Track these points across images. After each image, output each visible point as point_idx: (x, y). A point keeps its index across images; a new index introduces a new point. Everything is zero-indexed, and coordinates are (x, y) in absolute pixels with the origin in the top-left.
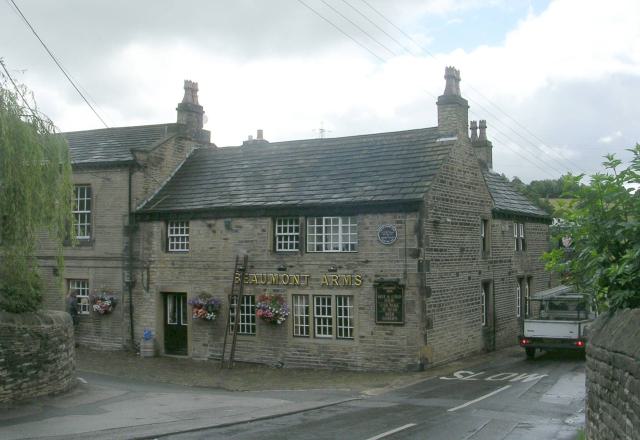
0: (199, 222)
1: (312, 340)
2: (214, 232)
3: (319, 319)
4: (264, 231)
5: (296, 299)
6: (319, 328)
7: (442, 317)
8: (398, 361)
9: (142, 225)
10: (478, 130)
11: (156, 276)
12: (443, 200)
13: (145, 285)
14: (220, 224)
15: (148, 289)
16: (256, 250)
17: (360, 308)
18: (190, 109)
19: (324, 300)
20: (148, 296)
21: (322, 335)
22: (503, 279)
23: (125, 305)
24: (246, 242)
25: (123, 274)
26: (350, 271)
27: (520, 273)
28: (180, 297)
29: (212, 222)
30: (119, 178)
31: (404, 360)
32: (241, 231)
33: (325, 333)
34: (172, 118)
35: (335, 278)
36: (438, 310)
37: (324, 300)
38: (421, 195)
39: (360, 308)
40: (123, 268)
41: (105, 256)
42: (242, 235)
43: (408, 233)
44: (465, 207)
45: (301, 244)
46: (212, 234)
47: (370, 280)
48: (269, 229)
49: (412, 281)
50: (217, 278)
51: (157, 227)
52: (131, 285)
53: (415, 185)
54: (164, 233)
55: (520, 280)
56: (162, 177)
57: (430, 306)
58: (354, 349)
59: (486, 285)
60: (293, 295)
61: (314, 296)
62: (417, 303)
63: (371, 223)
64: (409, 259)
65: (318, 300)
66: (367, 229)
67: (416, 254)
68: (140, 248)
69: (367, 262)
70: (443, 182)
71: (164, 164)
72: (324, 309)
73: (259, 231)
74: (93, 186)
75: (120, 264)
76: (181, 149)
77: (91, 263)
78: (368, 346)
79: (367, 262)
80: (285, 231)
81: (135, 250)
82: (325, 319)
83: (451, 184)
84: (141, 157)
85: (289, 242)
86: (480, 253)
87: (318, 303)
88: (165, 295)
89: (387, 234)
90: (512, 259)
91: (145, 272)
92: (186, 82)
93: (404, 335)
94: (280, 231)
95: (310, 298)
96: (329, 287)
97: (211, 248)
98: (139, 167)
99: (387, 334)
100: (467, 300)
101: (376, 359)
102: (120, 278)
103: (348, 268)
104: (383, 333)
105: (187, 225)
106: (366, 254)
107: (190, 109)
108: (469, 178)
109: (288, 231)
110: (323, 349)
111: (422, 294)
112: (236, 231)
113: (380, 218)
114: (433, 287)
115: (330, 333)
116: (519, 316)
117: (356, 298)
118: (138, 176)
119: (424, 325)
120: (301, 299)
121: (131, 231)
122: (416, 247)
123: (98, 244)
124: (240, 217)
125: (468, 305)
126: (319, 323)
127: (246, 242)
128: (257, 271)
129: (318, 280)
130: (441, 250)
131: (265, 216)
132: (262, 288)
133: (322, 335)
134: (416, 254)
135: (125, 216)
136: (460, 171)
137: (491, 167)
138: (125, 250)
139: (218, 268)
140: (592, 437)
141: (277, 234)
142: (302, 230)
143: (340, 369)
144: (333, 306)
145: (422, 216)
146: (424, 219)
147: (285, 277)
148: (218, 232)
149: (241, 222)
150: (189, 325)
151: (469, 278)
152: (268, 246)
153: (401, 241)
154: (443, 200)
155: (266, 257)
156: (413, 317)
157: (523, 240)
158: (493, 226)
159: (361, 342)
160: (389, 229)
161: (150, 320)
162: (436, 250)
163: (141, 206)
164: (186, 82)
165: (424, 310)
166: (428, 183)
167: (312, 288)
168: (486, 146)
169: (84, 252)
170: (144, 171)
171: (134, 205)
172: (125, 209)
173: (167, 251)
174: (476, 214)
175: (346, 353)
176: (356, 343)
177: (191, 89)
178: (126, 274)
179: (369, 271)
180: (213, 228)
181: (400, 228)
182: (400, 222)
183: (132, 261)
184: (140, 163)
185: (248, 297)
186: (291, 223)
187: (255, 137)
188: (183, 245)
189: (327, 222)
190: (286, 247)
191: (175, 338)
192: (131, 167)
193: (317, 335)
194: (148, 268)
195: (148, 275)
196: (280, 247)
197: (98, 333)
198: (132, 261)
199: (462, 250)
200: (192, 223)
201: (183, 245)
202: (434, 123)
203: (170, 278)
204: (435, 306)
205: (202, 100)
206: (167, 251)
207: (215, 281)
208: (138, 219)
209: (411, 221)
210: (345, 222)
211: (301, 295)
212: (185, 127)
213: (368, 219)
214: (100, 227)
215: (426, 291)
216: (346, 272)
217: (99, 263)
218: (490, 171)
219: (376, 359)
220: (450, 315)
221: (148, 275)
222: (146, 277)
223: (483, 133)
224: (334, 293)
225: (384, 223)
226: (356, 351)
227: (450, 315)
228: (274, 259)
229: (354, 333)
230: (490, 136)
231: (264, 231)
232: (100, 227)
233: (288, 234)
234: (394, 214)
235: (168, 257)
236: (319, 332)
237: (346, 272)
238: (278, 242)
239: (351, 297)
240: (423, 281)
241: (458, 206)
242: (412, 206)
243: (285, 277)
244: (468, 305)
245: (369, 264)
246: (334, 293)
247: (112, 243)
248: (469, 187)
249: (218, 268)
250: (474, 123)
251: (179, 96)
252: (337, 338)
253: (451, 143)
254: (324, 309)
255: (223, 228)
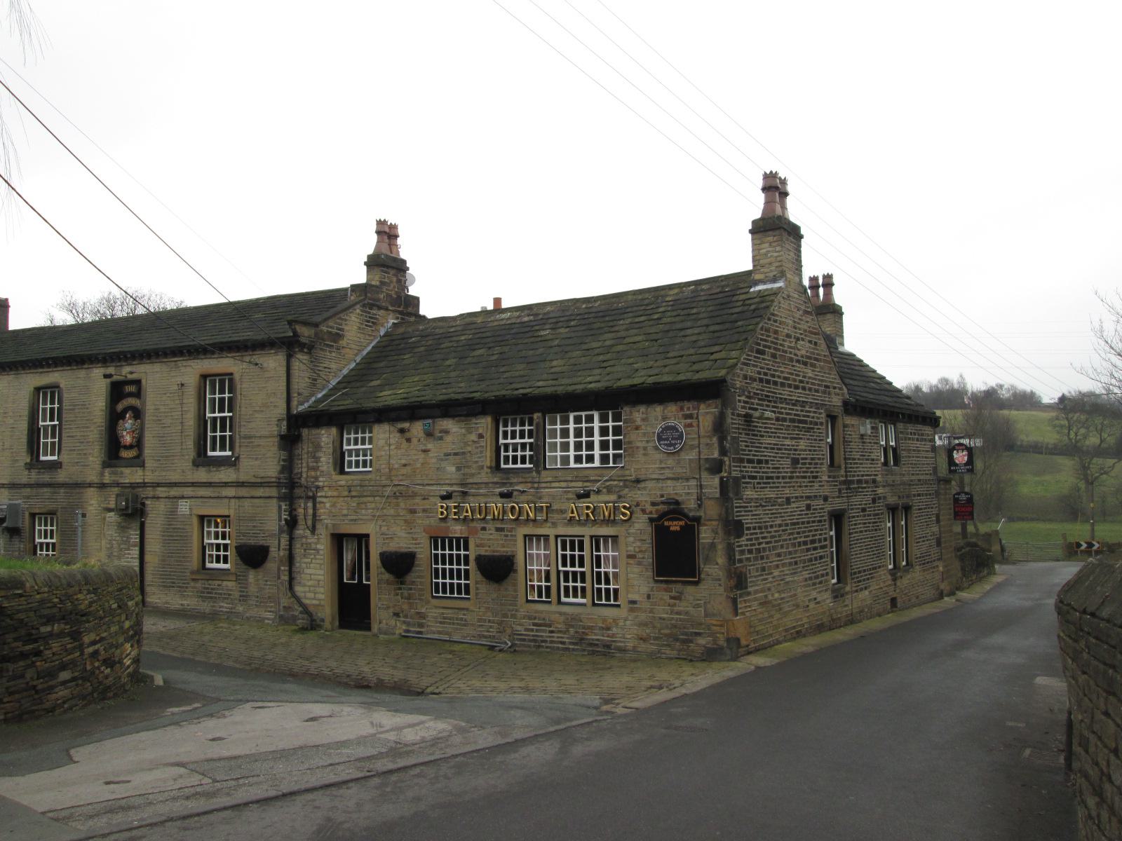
0: (386, 427)
1: (554, 607)
2: (409, 440)
3: (566, 573)
4: (481, 436)
5: (531, 540)
6: (567, 588)
7: (763, 569)
8: (691, 641)
9: (305, 432)
10: (821, 290)
11: (325, 507)
12: (761, 380)
13: (310, 523)
14: (417, 428)
15: (313, 530)
16: (469, 467)
17: (629, 557)
18: (387, 263)
19: (572, 543)
20: (312, 540)
21: (571, 600)
22: (864, 510)
23: (282, 553)
24: (456, 454)
25: (280, 507)
26: (613, 497)
27: (892, 500)
28: (362, 539)
29: (406, 425)
30: (274, 362)
31: (702, 641)
32: (449, 438)
33: (575, 596)
34: (359, 276)
35: (588, 508)
36: (756, 559)
37: (572, 543)
38: (723, 373)
39: (629, 557)
40: (280, 498)
41: (253, 480)
42: (450, 443)
43: (702, 433)
44: (797, 395)
45: (538, 459)
46: (405, 444)
47: (644, 511)
48: (489, 435)
49: (712, 510)
50: (413, 512)
51: (326, 436)
52: (292, 523)
53: (713, 357)
54: (337, 444)
55: (893, 510)
56: (339, 365)
57: (742, 552)
58: (621, 623)
59: (838, 518)
60: (525, 536)
61: (557, 537)
62: (720, 547)
63: (643, 420)
64: (705, 475)
65: (564, 543)
66: (637, 428)
67: (716, 467)
68: (302, 468)
69: (638, 481)
70: (763, 353)
71: (343, 343)
72: (573, 557)
73: (473, 437)
74: (237, 377)
75: (273, 492)
76: (373, 322)
77: (230, 492)
78: (643, 617)
79: (638, 481)
80: (513, 437)
81: (296, 471)
82: (574, 573)
83: (774, 356)
84: (305, 332)
85: (519, 453)
86: (825, 468)
87: (564, 549)
88: (339, 540)
89: (669, 436)
90: (879, 478)
91: (310, 505)
92: (381, 223)
93: (707, 595)
94: (505, 437)
95: (552, 540)
96: (580, 523)
97: (405, 465)
98: (302, 346)
99: (672, 598)
100: (805, 543)
101: (656, 638)
102: (273, 514)
103: (610, 490)
104: (666, 596)
105: (371, 432)
106: (636, 470)
107: (387, 263)
108: (804, 348)
109: (515, 437)
110: (572, 621)
111: (728, 533)
112: (441, 438)
113: (658, 410)
114: (747, 520)
115: (584, 596)
116: (891, 567)
117: (621, 539)
118: (301, 362)
119: (733, 583)
120: (606, 542)
121: (290, 440)
122: (716, 455)
123: (245, 463)
124: (446, 415)
125: (808, 550)
126: (566, 580)
127: (456, 454)
128: (471, 499)
129: (562, 512)
130: (760, 462)
131: (483, 413)
132: (479, 525)
133: (571, 600)
134: (716, 467)
135: (283, 420)
136: (788, 336)
137: (842, 344)
138: (281, 472)
139: (414, 495)
140: (1087, 836)
141: (502, 441)
142: (539, 434)
143: (597, 651)
144: (586, 553)
145: (724, 405)
146: (729, 411)
147: (513, 508)
148: (414, 441)
149: (448, 424)
150: (373, 583)
151: (808, 507)
152: (488, 460)
153: (692, 447)
154: (761, 380)
155: (485, 476)
156: (714, 569)
157: (895, 450)
158: (845, 426)
159: (631, 610)
160: (674, 428)
161: (316, 581)
162: (750, 461)
163: (306, 405)
164: (381, 223)
165: (731, 558)
166: (734, 354)
167: (554, 525)
168: (833, 312)
169: (226, 475)
170: (309, 353)
171: (294, 403)
172: (281, 410)
173: (342, 472)
174: (818, 406)
175: (608, 629)
176: (622, 613)
177: (387, 233)
178: (284, 507)
179: (643, 496)
180: (407, 435)
181: (690, 425)
182: (690, 416)
183: (291, 488)
184: (303, 340)
185: (458, 540)
186: (522, 424)
187: (490, 307)
188: (365, 462)
189: (578, 420)
190: (515, 462)
191: (353, 607)
192: (290, 345)
193: (563, 599)
194: (314, 498)
195: (315, 508)
196: (506, 462)
197: (244, 598)
198: (291, 488)
199: (795, 462)
200: (376, 428)
201: (365, 462)
202: (747, 265)
203: (345, 512)
204: (750, 552)
205: (406, 249)
206: (342, 472)
207: (409, 517)
208: (296, 428)
209: (706, 413)
210: (604, 419)
211: (539, 537)
212: (377, 289)
213: (638, 414)
214: (245, 437)
215: (734, 528)
216: (607, 498)
217: (243, 492)
218: (841, 349)
219: (656, 638)
220: (777, 566)
221: (315, 508)
222: (310, 511)
223: (828, 293)
224: (587, 531)
225: (664, 418)
226: (623, 625)
227: (777, 566)
228: (495, 480)
229: (621, 594)
230: (839, 296)
231: (481, 436)
232: (245, 437)
233: (518, 440)
234: (679, 404)
235: (343, 480)
236: (567, 595)
237: (607, 498)
238: (503, 454)
239: (615, 538)
240: (728, 511)
241: (785, 393)
242: (711, 390)
243: (513, 508)
244: (808, 550)
245: (642, 485)
246: (587, 531)
247: (263, 461)
248: (805, 364)
249: (414, 495)
250: (814, 279)
251: (369, 244)
252: (594, 604)
253: (775, 293)
254: (573, 557)
255: (421, 435)
